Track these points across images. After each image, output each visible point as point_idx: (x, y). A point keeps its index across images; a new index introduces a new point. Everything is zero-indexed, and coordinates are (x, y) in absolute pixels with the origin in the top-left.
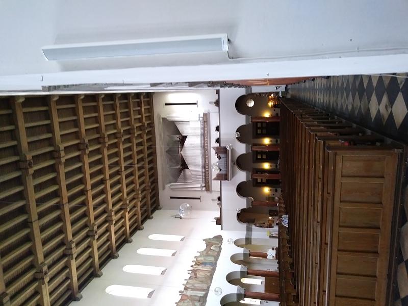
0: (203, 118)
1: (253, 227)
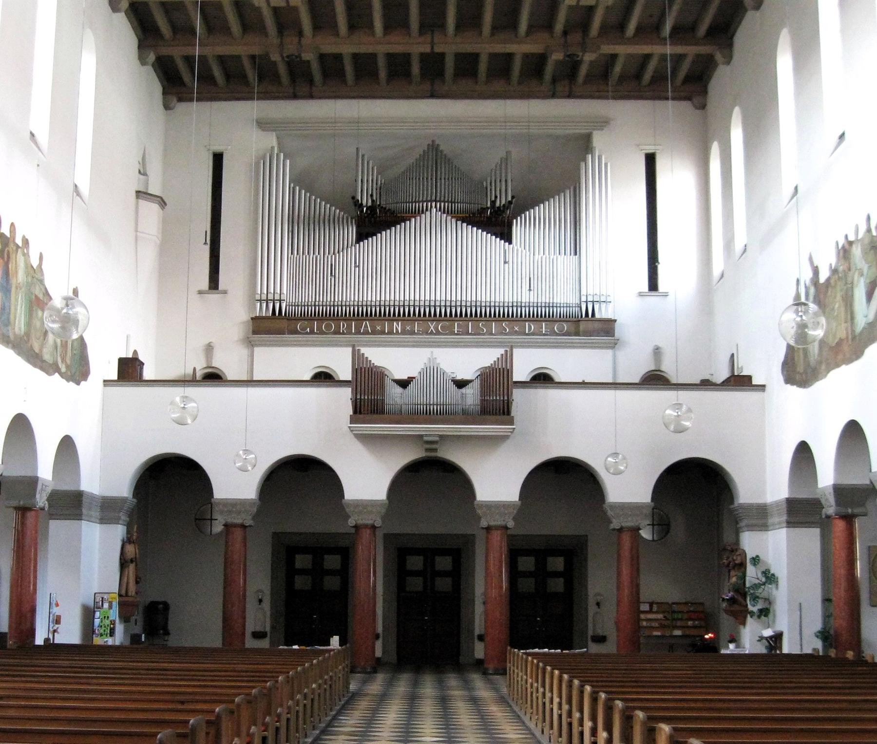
0: (589, 316)
1: (118, 532)
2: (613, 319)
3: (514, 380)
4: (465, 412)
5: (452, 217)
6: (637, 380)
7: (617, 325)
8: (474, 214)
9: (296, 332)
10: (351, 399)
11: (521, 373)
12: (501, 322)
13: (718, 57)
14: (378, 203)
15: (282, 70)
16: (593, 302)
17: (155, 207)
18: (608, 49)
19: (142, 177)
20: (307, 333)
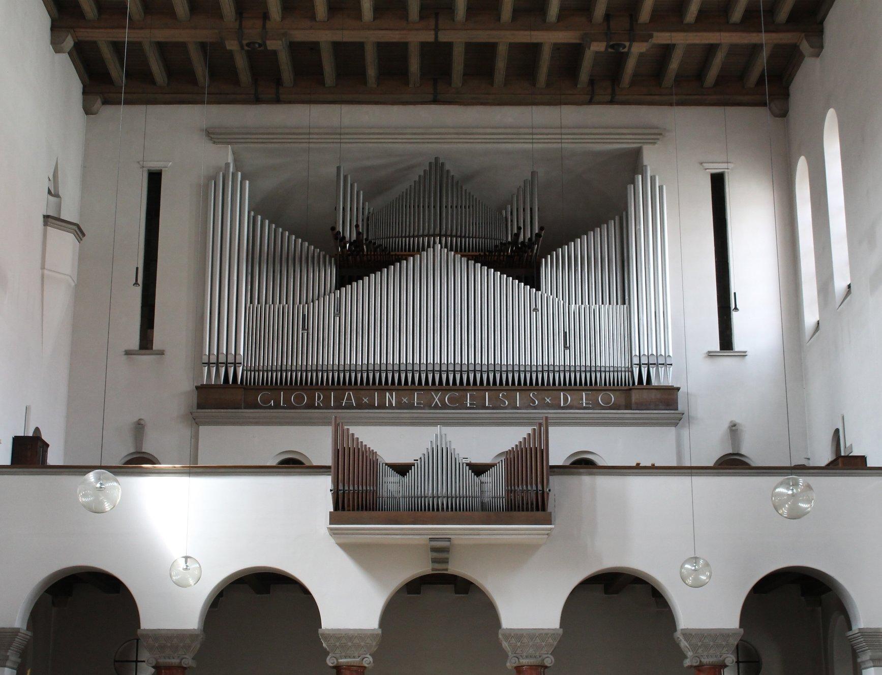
0: (645, 384)
2: (675, 386)
3: (550, 464)
4: (484, 507)
5: (462, 256)
6: (711, 464)
7: (680, 393)
8: (490, 252)
9: (255, 406)
10: (331, 490)
11: (558, 456)
12: (528, 392)
13: (805, 46)
14: (365, 237)
15: (241, 62)
16: (648, 365)
17: (69, 238)
18: (662, 38)
19: (51, 198)
20: (270, 407)
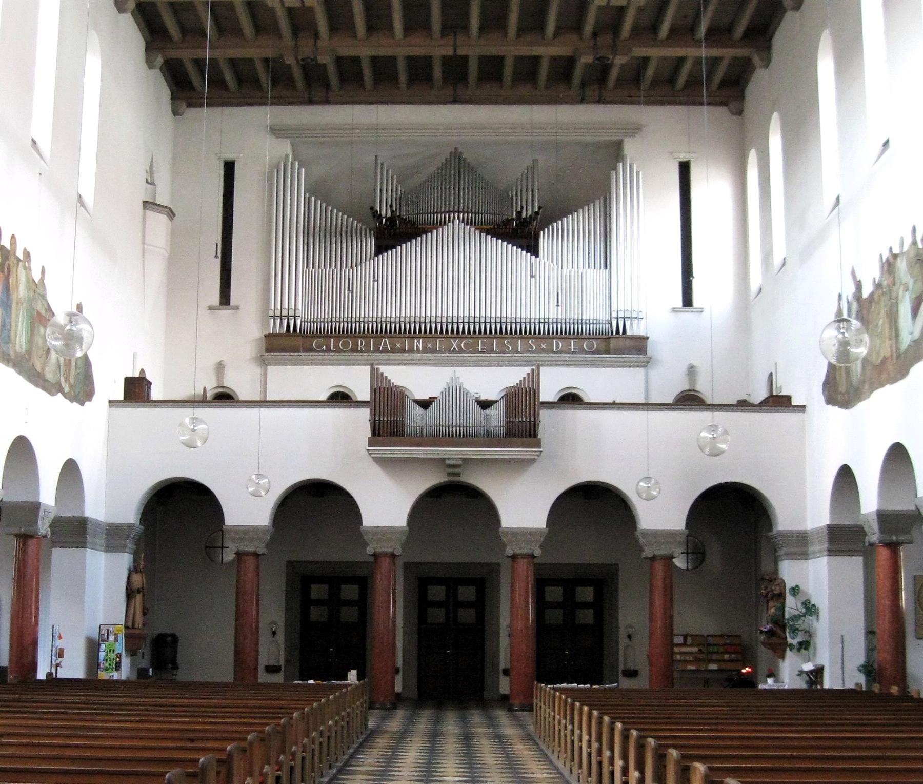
0: (620, 333)
1: (124, 560)
2: (645, 336)
3: (541, 401)
4: (489, 434)
5: (476, 229)
6: (670, 401)
7: (649, 342)
8: (499, 225)
9: (311, 350)
10: (370, 421)
11: (548, 393)
12: (527, 340)
13: (756, 60)
14: (398, 214)
15: (297, 73)
16: (624, 318)
17: (163, 218)
18: (639, 52)
19: (149, 186)
20: (323, 351)
